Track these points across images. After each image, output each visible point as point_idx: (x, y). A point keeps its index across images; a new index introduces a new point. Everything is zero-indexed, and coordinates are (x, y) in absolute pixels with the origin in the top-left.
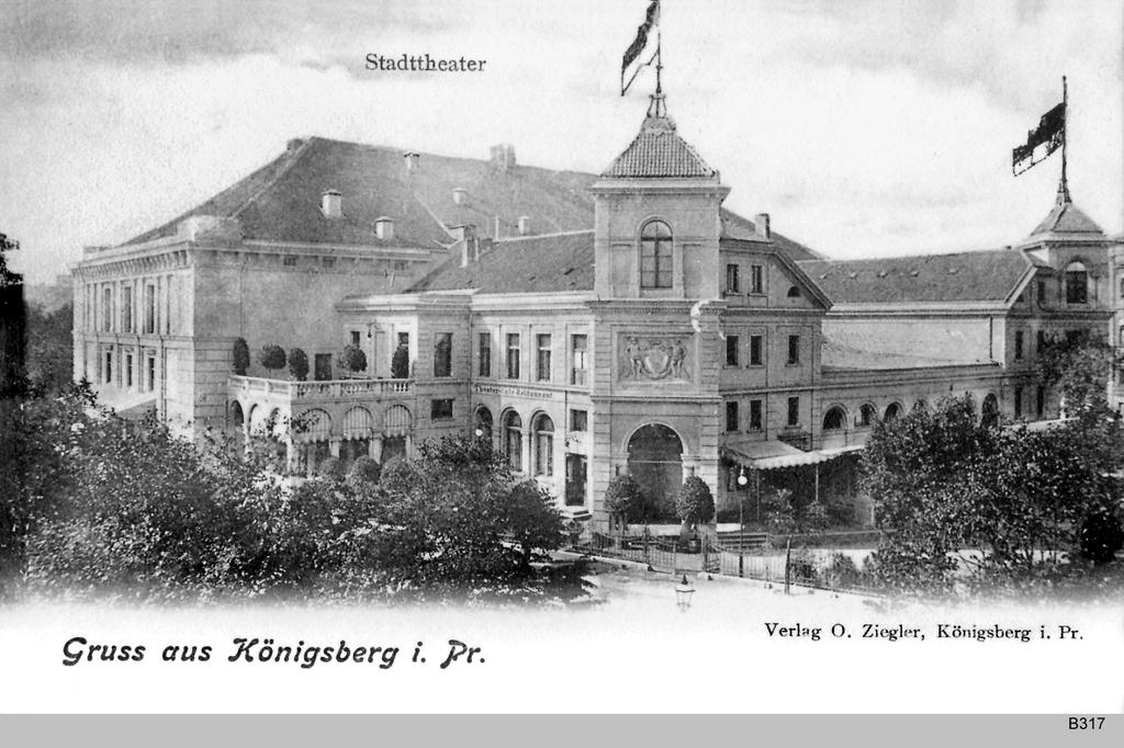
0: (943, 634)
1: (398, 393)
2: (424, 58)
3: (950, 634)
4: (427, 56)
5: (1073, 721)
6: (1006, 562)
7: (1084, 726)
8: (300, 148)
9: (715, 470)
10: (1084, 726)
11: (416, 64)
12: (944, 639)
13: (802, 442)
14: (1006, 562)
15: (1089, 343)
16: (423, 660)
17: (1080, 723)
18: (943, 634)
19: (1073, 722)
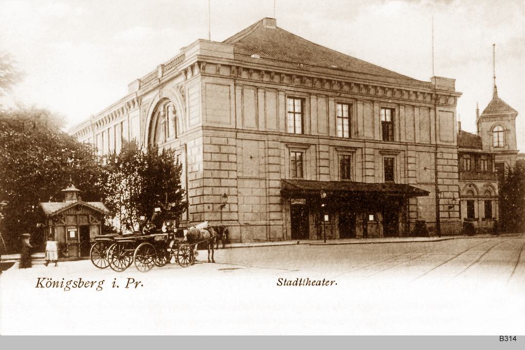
0: (39, 285)
1: (386, 146)
2: (306, 280)
3: (44, 284)
4: (308, 279)
5: (502, 337)
6: (68, 189)
7: (506, 340)
8: (72, 142)
9: (357, 234)
10: (506, 340)
11: (302, 282)
12: (40, 289)
13: (83, 223)
14: (68, 189)
15: (284, 199)
16: (118, 287)
17: (505, 338)
18: (39, 285)
19: (501, 338)
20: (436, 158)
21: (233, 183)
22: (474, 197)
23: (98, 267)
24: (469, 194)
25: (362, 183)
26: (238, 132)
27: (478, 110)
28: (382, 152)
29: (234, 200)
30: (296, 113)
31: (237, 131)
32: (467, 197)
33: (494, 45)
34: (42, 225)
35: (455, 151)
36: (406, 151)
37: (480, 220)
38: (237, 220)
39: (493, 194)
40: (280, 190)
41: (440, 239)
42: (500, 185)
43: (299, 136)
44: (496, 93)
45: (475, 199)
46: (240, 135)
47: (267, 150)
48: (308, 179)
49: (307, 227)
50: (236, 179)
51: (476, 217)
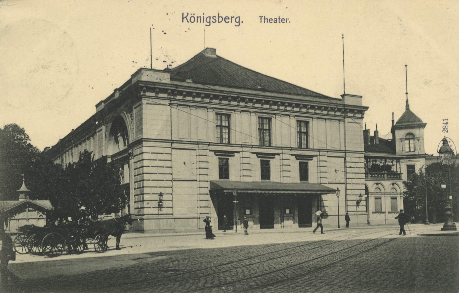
20: (346, 162)
21: (169, 184)
22: (397, 193)
23: (24, 254)
24: (393, 191)
25: (281, 183)
26: (173, 143)
27: (393, 121)
28: (298, 157)
29: (169, 198)
30: (223, 126)
31: (172, 142)
32: (390, 193)
33: (406, 66)
34: (95, 217)
35: (363, 156)
36: (318, 157)
37: (387, 213)
38: (172, 214)
39: (399, 191)
40: (209, 189)
41: (162, 235)
42: (36, 151)
43: (226, 145)
44: (407, 106)
45: (398, 195)
46: (175, 145)
47: (282, 166)
48: (233, 180)
49: (278, 221)
50: (171, 181)
51: (383, 210)
